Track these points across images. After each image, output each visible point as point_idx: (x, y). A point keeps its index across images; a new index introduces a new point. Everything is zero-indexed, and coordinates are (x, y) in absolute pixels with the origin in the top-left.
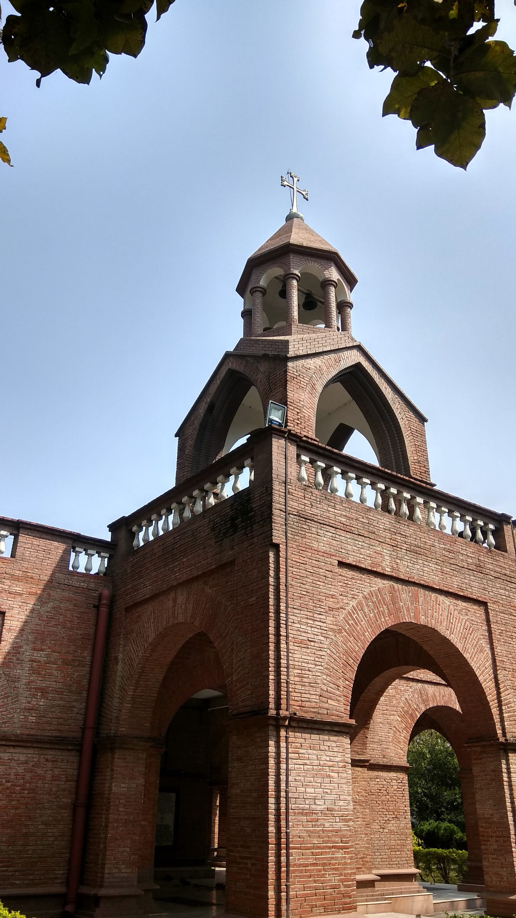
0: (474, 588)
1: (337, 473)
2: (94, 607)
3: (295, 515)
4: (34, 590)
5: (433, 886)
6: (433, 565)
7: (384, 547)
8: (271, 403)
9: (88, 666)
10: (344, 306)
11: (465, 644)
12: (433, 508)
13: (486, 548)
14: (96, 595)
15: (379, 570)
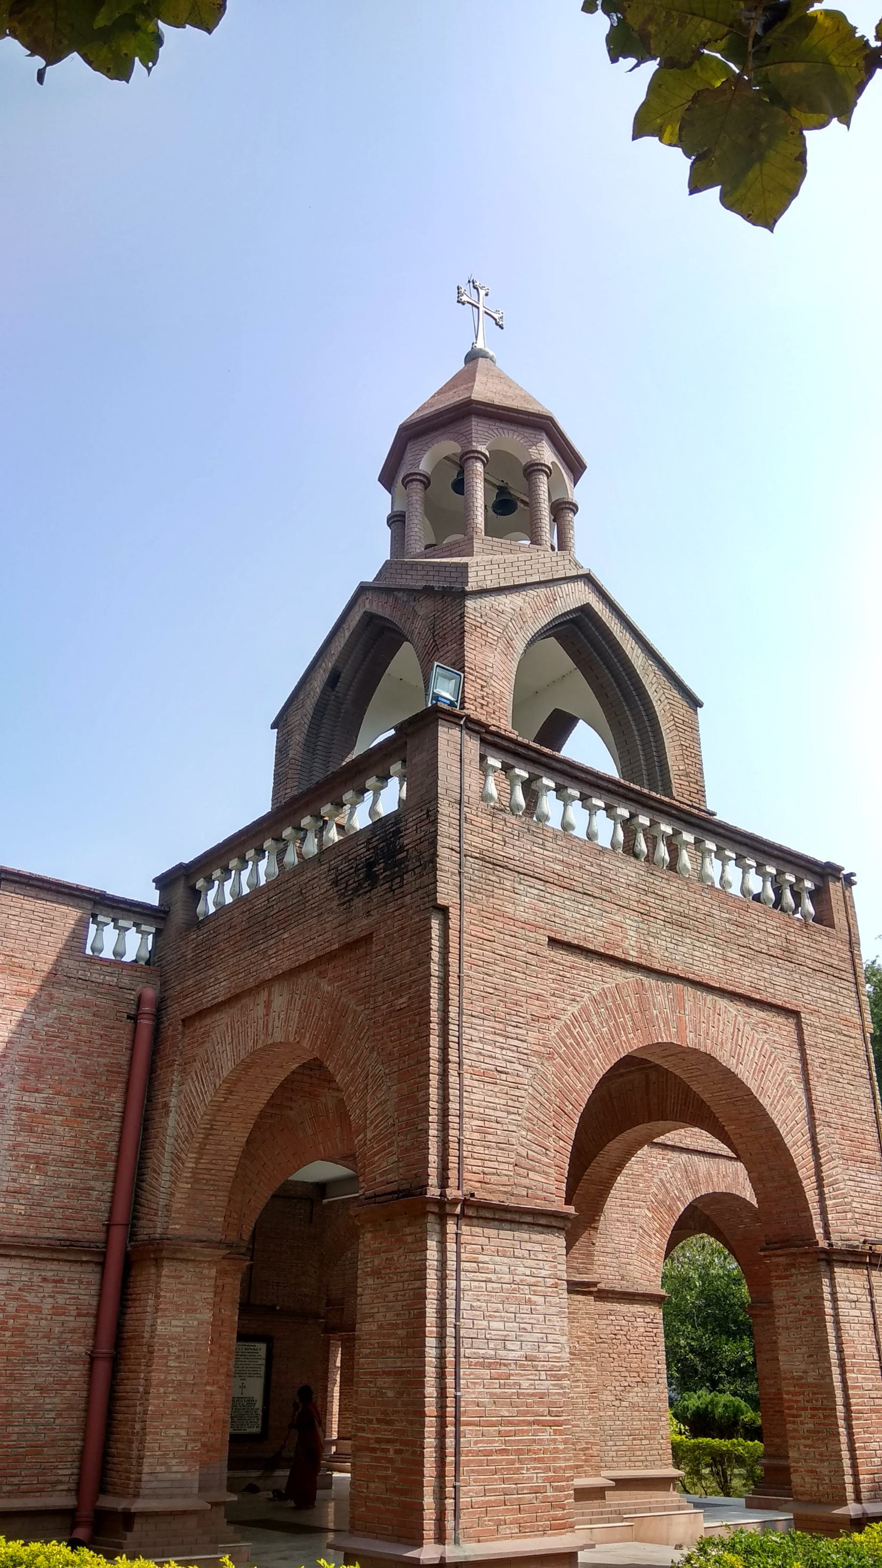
0: (777, 988)
1: (548, 789)
2: (129, 1017)
3: (476, 858)
4: (24, 988)
5: (703, 1500)
6: (710, 948)
7: (628, 916)
8: (438, 666)
10: (562, 509)
11: (761, 1080)
12: (710, 851)
13: (798, 920)
14: (132, 997)
15: (618, 953)
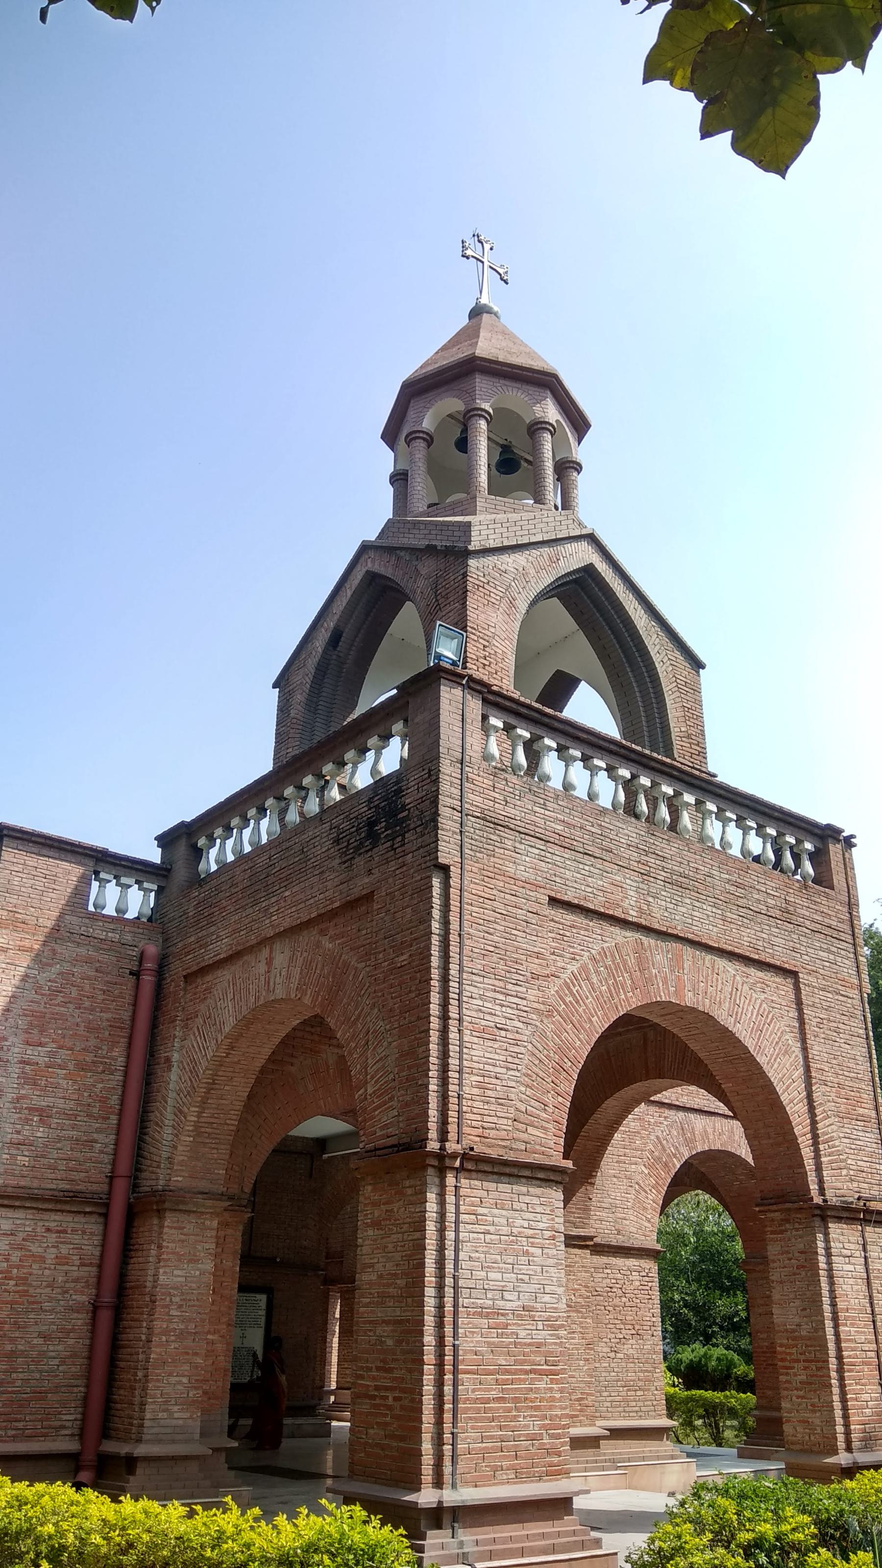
0: (776, 948)
1: (550, 749)
2: (131, 974)
3: (478, 817)
4: (27, 943)
5: (696, 1450)
6: (709, 908)
7: (628, 876)
9: (120, 1073)
10: (566, 468)
11: (759, 1039)
12: (711, 812)
13: (798, 881)
14: (134, 954)
15: (618, 913)
